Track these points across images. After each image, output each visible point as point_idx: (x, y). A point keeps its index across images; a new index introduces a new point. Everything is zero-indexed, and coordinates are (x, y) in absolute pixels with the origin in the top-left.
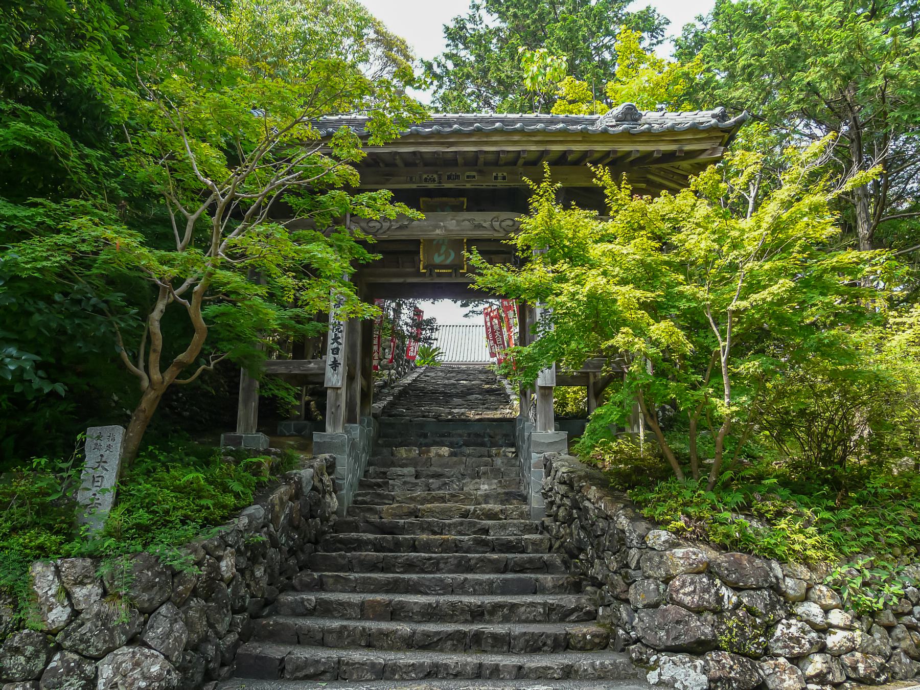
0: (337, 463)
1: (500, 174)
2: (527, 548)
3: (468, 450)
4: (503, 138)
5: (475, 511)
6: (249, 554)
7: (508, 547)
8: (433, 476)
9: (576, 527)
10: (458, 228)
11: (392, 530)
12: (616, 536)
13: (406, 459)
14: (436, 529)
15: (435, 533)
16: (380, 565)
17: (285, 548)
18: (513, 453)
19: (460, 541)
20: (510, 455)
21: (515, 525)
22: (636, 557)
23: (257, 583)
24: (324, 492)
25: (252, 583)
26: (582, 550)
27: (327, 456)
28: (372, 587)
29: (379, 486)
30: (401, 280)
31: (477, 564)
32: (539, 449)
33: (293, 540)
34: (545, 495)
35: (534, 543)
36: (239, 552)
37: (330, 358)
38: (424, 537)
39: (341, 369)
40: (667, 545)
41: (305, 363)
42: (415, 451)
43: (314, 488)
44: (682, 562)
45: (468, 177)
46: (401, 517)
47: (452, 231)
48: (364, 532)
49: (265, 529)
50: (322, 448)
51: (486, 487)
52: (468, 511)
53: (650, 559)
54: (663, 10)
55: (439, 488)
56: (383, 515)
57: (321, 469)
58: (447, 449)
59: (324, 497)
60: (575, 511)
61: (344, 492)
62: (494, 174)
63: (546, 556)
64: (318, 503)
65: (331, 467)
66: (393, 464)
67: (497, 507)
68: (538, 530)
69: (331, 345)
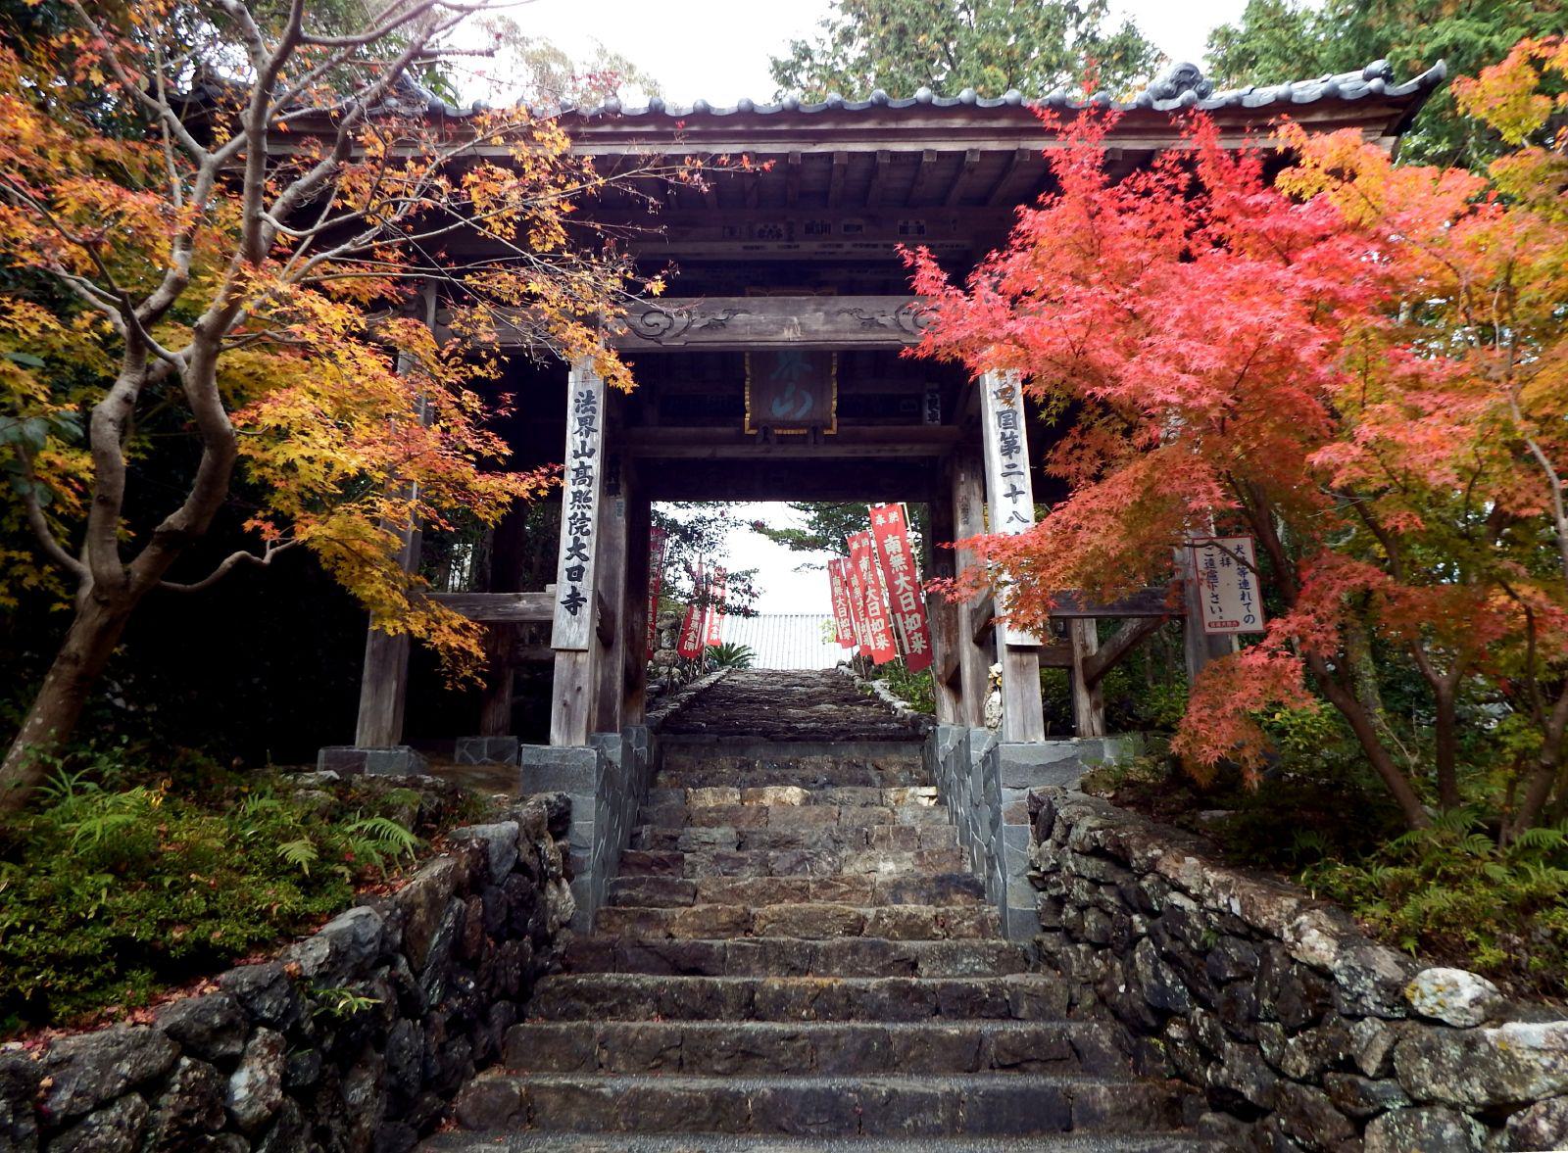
0: (574, 814)
1: (911, 223)
2: (1018, 1006)
3: (840, 794)
4: (933, 124)
5: (878, 918)
6: (328, 1043)
7: (966, 1003)
8: (774, 845)
9: (1145, 956)
10: (829, 327)
11: (694, 962)
12: (1298, 983)
13: (718, 809)
14: (797, 962)
15: (794, 970)
16: (674, 1054)
17: (439, 1018)
18: (932, 798)
19: (860, 992)
20: (925, 802)
21: (975, 952)
22: (1382, 1044)
23: (351, 1123)
24: (544, 877)
25: (336, 1125)
26: (1165, 1015)
27: (552, 796)
28: (658, 1116)
29: (663, 864)
30: (704, 452)
31: (908, 1048)
32: (1017, 781)
33: (464, 994)
34: (1039, 882)
35: (1033, 995)
36: (295, 1039)
37: (562, 588)
38: (775, 983)
39: (586, 610)
40: (1479, 1011)
41: (508, 600)
42: (733, 797)
43: (520, 867)
44: (1546, 1061)
45: (847, 228)
46: (714, 933)
47: (817, 332)
48: (634, 969)
49: (385, 971)
50: (539, 778)
51: (890, 866)
52: (861, 920)
53: (1430, 1050)
54: (1150, 33)
55: (791, 870)
56: (674, 930)
57: (537, 825)
58: (797, 790)
59: (542, 889)
60: (1136, 918)
61: (588, 877)
62: (901, 223)
63: (1074, 1030)
64: (531, 903)
65: (559, 821)
66: (689, 821)
67: (927, 912)
68: (1028, 962)
69: (565, 562)
